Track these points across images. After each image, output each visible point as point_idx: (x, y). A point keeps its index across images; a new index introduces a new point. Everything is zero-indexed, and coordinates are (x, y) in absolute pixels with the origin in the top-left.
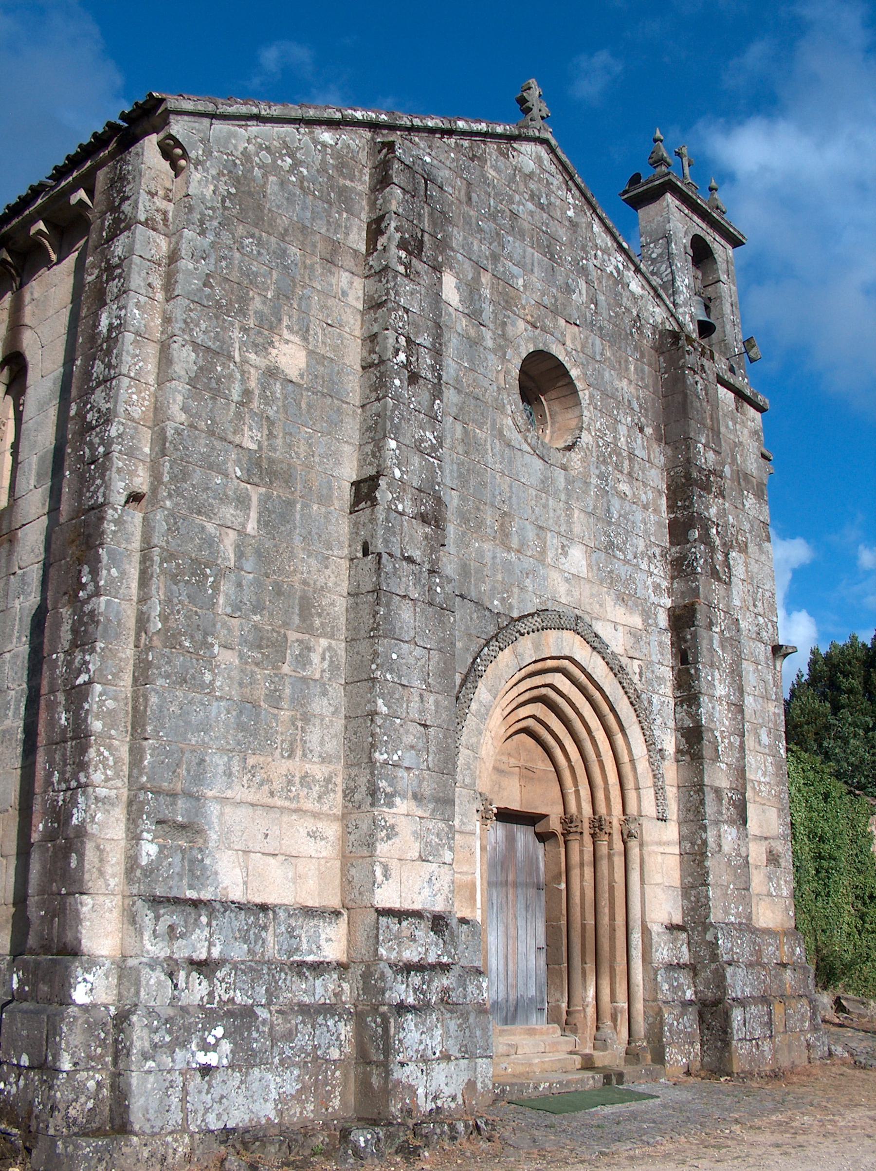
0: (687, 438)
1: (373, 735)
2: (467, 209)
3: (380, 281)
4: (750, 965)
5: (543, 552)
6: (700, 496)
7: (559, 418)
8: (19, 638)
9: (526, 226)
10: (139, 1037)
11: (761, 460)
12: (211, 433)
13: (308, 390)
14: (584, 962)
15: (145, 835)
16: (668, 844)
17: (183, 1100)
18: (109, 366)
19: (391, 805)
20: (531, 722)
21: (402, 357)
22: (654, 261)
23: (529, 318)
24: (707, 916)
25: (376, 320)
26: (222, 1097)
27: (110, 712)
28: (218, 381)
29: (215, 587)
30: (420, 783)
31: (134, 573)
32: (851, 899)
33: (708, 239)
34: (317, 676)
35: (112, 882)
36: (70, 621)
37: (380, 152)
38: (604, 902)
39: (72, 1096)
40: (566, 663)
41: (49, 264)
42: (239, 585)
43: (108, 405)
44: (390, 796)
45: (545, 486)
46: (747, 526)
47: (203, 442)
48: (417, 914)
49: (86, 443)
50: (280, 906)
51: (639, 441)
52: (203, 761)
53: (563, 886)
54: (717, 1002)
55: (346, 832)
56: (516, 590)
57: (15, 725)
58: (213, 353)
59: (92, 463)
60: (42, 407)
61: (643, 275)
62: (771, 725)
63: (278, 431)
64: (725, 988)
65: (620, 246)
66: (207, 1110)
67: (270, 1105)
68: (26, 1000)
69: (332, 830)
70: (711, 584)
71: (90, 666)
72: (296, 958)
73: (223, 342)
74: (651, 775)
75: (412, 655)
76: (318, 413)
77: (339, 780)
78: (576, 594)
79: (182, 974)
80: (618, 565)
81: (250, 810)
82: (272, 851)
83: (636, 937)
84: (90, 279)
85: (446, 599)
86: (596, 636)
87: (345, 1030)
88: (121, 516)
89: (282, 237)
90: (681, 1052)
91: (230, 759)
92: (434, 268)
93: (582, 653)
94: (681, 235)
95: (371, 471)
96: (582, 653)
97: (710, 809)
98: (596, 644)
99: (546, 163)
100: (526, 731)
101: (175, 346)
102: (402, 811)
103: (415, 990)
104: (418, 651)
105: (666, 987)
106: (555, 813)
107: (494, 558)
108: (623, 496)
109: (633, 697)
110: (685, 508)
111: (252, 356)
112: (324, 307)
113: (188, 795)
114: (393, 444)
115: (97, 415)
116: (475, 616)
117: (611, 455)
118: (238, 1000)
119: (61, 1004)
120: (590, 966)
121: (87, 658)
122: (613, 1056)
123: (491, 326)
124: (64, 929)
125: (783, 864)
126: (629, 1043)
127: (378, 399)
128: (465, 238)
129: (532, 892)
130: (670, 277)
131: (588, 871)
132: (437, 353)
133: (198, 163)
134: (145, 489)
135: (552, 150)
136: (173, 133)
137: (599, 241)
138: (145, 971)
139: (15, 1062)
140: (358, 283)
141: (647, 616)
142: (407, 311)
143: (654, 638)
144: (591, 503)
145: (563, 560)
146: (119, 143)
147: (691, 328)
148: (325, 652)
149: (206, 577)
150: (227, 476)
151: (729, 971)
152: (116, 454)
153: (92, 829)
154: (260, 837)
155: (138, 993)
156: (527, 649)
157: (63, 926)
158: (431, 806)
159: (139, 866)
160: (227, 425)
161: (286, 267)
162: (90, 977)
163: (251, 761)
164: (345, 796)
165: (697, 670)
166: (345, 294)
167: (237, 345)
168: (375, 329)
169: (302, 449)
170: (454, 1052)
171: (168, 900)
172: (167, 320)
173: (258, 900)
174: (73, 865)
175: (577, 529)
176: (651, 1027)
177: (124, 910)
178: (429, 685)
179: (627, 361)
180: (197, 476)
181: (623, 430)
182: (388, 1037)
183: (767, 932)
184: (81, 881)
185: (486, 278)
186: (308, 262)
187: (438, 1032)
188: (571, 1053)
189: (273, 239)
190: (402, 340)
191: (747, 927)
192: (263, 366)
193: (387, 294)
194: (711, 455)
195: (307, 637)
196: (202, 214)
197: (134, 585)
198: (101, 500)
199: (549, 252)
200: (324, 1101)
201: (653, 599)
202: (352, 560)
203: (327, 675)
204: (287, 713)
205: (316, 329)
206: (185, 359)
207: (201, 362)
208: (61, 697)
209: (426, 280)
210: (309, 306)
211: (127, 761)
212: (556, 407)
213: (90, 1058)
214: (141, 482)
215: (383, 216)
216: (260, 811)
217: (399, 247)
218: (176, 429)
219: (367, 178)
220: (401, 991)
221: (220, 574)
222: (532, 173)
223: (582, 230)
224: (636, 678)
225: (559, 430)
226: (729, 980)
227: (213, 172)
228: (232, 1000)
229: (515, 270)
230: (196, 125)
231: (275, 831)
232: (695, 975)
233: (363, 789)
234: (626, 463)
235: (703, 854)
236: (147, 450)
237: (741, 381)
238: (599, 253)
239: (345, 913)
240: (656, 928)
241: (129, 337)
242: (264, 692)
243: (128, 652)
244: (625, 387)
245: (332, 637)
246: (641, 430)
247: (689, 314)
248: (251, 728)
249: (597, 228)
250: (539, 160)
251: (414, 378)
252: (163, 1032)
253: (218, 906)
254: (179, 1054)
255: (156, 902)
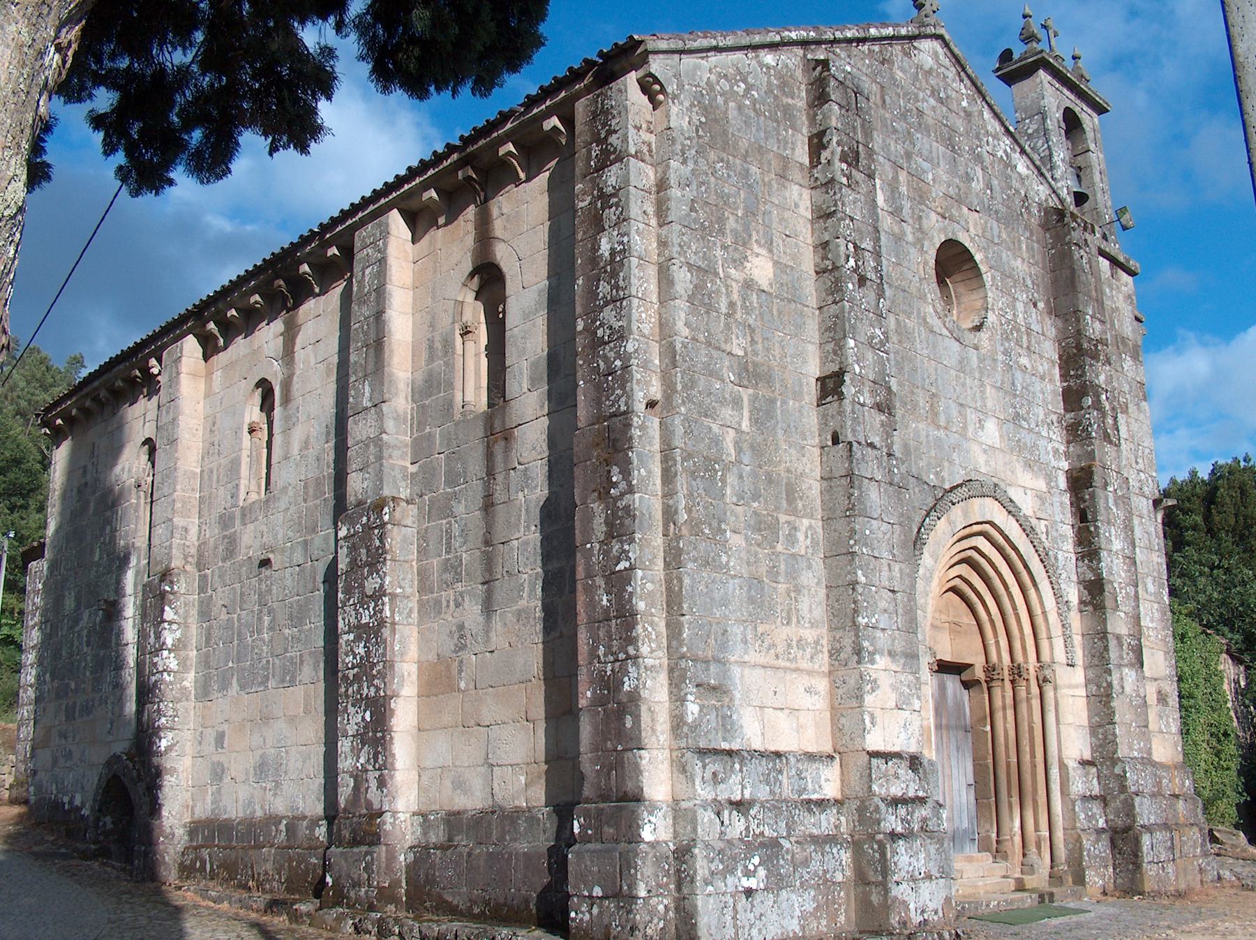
0: (1076, 311)
1: (855, 602)
2: (883, 112)
3: (827, 193)
4: (1153, 795)
5: (965, 428)
6: (1091, 365)
7: (964, 299)
8: (528, 527)
9: (930, 121)
10: (701, 867)
11: (1135, 323)
12: (709, 344)
13: (777, 297)
14: (1010, 796)
15: (690, 697)
16: (1076, 687)
17: (734, 918)
18: (617, 288)
19: (872, 662)
20: (958, 582)
21: (852, 262)
22: (1030, 137)
23: (939, 210)
24: (1115, 752)
25: (826, 229)
26: (761, 915)
27: (651, 593)
28: (710, 296)
29: (723, 480)
30: (893, 641)
31: (657, 471)
32: (1207, 737)
33: (1077, 110)
34: (803, 552)
35: (662, 738)
36: (603, 516)
37: (814, 69)
38: (1025, 742)
39: (648, 918)
40: (987, 527)
41: (517, 182)
42: (741, 477)
43: (620, 323)
44: (871, 654)
45: (962, 366)
46: (1126, 388)
47: (703, 352)
48: (898, 755)
49: (599, 356)
50: (790, 752)
51: (1034, 316)
52: (726, 631)
53: (988, 728)
54: (1128, 829)
55: (834, 686)
56: (946, 464)
57: (533, 604)
58: (704, 272)
59: (610, 374)
60: (526, 316)
61: (1027, 155)
62: (1155, 574)
63: (758, 338)
64: (1134, 816)
65: (1007, 130)
66: (751, 926)
67: (795, 921)
68: (590, 842)
69: (822, 685)
70: (1104, 447)
71: (630, 554)
72: (804, 797)
73: (710, 261)
74: (1060, 625)
75: (880, 531)
76: (786, 318)
77: (824, 642)
78: (992, 463)
79: (726, 812)
80: (1024, 433)
81: (762, 671)
82: (780, 708)
83: (1055, 772)
84: (581, 205)
85: (902, 478)
86: (1011, 501)
87: (846, 856)
88: (643, 422)
89: (745, 158)
90: (1098, 874)
91: (745, 628)
92: (869, 176)
93: (1001, 518)
94: (1054, 109)
95: (835, 368)
96: (1001, 518)
97: (1113, 654)
98: (1010, 509)
99: (942, 57)
100: (954, 590)
101: (675, 268)
102: (881, 668)
103: (902, 820)
104: (885, 527)
105: (1082, 816)
106: (978, 662)
107: (928, 436)
108: (1024, 369)
109: (1043, 555)
110: (1077, 377)
111: (733, 271)
112: (782, 220)
113: (718, 661)
114: (851, 343)
115: (608, 332)
116: (917, 490)
117: (1012, 332)
118: (766, 833)
119: (630, 843)
120: (1015, 800)
121: (626, 547)
122: (1039, 879)
123: (910, 221)
124: (623, 780)
125: (1171, 703)
126: (1052, 867)
127: (835, 302)
128: (884, 141)
129: (961, 734)
130: (1047, 153)
131: (1010, 713)
132: (877, 255)
133: (675, 97)
134: (658, 396)
135: (946, 45)
136: (653, 71)
137: (989, 128)
138: (700, 811)
139: (586, 893)
140: (806, 193)
141: (1050, 478)
142: (852, 219)
143: (1056, 499)
144: (999, 378)
145: (980, 433)
146: (595, 76)
147: (1069, 200)
148: (808, 531)
149: (716, 471)
150: (723, 381)
151: (1137, 800)
152: (635, 368)
153: (644, 694)
154: (772, 694)
155: (695, 830)
156: (957, 517)
157: (621, 778)
158: (902, 661)
159: (685, 723)
160: (720, 335)
161: (750, 186)
162: (653, 819)
163: (760, 629)
164: (831, 656)
165: (1097, 527)
166: (796, 206)
167: (720, 263)
168: (826, 237)
169: (777, 351)
170: (935, 873)
171: (709, 751)
172: (663, 244)
173: (773, 749)
174: (629, 724)
175: (990, 404)
176: (1070, 852)
177: (672, 761)
178: (894, 556)
179: (1019, 241)
180: (702, 383)
181: (1020, 306)
182: (886, 860)
183: (1162, 766)
184: (639, 739)
185: (903, 176)
186: (766, 179)
187: (922, 856)
188: (1004, 877)
189: (738, 162)
190: (851, 246)
191: (1147, 761)
192: (741, 279)
193: (836, 205)
194: (1097, 325)
195: (793, 518)
196: (683, 145)
197: (659, 482)
198: (623, 408)
199: (951, 145)
200: (833, 918)
201: (1054, 463)
202: (823, 448)
203: (810, 551)
204: (785, 586)
205: (777, 241)
206: (683, 279)
207: (695, 281)
208: (600, 581)
209: (864, 188)
210: (770, 220)
211: (665, 634)
212: (961, 289)
213: (659, 886)
214: (656, 391)
215: (824, 132)
216: (769, 672)
217: (841, 160)
218: (683, 343)
219: (804, 94)
220: (892, 821)
221: (726, 469)
222: (931, 68)
223: (975, 119)
224: (1043, 537)
225: (965, 310)
226: (1137, 810)
227: (687, 104)
228: (762, 833)
229: (926, 165)
230: (669, 62)
231: (781, 689)
232: (1106, 805)
233: (849, 649)
234: (1025, 337)
235: (1109, 696)
236: (657, 362)
237: (1113, 248)
238: (990, 139)
239: (837, 756)
240: (1072, 764)
241: (634, 261)
242: (765, 569)
243: (658, 541)
244: (1020, 266)
245: (812, 517)
246: (1035, 305)
247: (1066, 185)
248: (759, 604)
249: (987, 115)
250: (935, 55)
251: (862, 281)
252: (717, 862)
253: (745, 754)
254: (730, 879)
255: (703, 753)
